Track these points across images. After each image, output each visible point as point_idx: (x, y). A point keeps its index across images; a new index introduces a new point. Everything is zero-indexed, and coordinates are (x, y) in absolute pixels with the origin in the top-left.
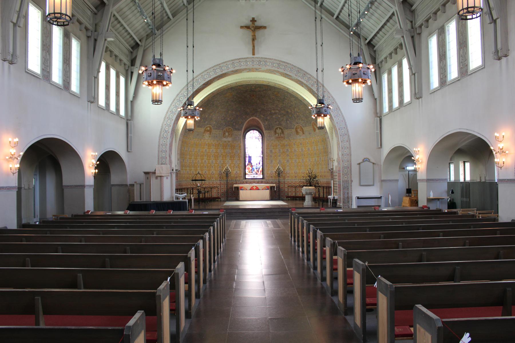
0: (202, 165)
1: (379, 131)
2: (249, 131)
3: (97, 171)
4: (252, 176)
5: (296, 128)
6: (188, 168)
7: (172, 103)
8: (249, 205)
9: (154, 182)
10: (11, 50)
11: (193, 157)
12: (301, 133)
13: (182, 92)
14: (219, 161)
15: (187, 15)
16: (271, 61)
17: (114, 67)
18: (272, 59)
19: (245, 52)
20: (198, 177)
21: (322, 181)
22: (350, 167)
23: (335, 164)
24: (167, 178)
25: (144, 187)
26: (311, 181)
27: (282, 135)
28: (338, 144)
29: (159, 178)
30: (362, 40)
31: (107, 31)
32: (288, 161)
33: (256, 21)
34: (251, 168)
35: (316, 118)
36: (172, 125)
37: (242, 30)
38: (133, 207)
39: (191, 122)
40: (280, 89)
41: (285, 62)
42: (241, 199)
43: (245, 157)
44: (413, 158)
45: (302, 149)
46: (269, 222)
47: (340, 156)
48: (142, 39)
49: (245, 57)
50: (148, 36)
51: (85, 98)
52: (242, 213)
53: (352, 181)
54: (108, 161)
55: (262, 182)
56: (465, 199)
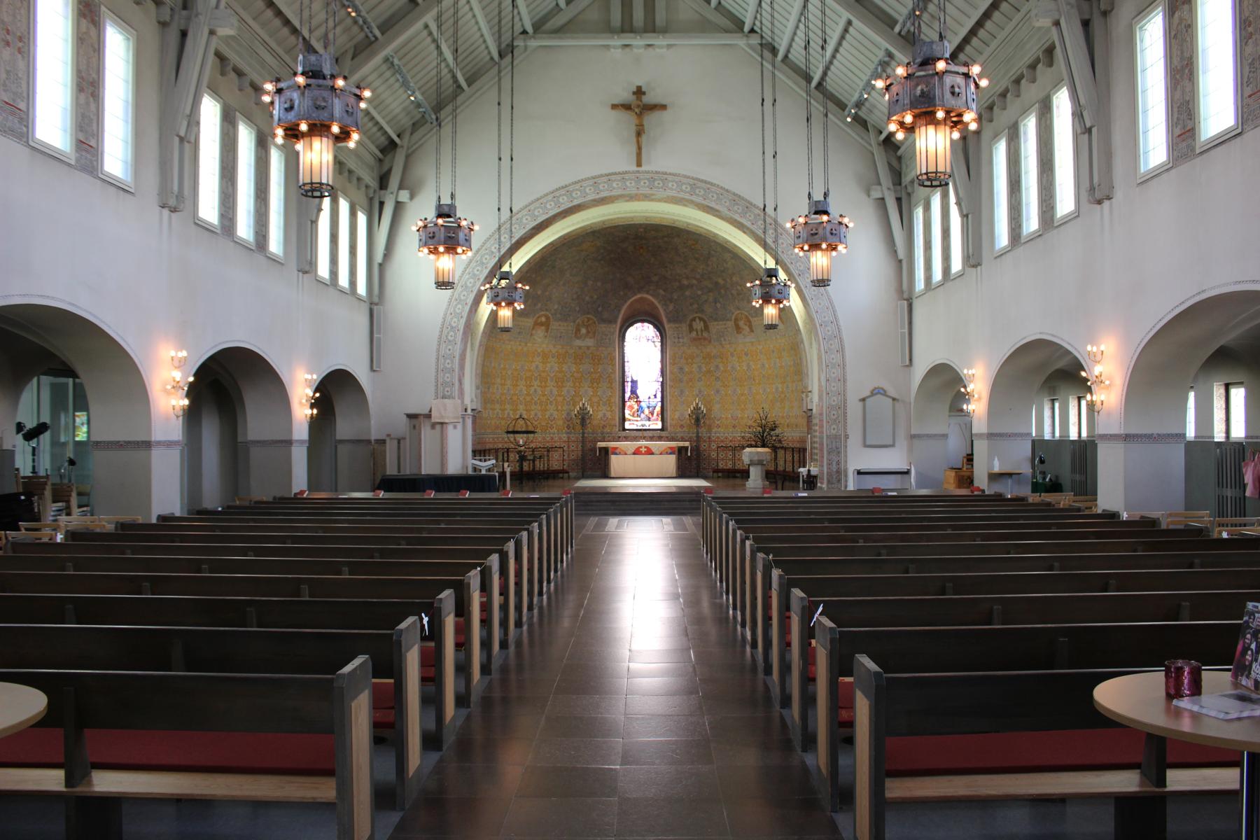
0: (528, 399)
1: (906, 330)
2: (632, 324)
3: (315, 411)
4: (640, 423)
5: (736, 320)
6: (497, 406)
7: (466, 269)
8: (628, 487)
9: (428, 436)
10: (176, 188)
11: (509, 382)
12: (747, 328)
13: (488, 245)
14: (565, 390)
15: (500, 80)
16: (677, 179)
17: (346, 195)
18: (678, 175)
19: (617, 158)
20: (520, 425)
21: (790, 435)
22: (843, 407)
23: (815, 397)
24: (455, 427)
25: (406, 445)
26: (765, 436)
27: (705, 334)
28: (820, 358)
29: (438, 427)
30: (872, 134)
31: (217, 7)
32: (718, 391)
33: (644, 93)
34: (636, 407)
35: (762, 306)
36: (465, 315)
37: (614, 112)
38: (389, 484)
39: (505, 313)
40: (700, 235)
41: (705, 182)
42: (613, 475)
43: (623, 382)
44: (1083, 374)
45: (748, 366)
46: (667, 520)
47: (823, 383)
48: (404, 131)
49: (621, 170)
50: (415, 126)
51: (293, 265)
52: (613, 502)
53: (847, 437)
54: (335, 389)
55: (660, 438)
56: (1078, 477)
